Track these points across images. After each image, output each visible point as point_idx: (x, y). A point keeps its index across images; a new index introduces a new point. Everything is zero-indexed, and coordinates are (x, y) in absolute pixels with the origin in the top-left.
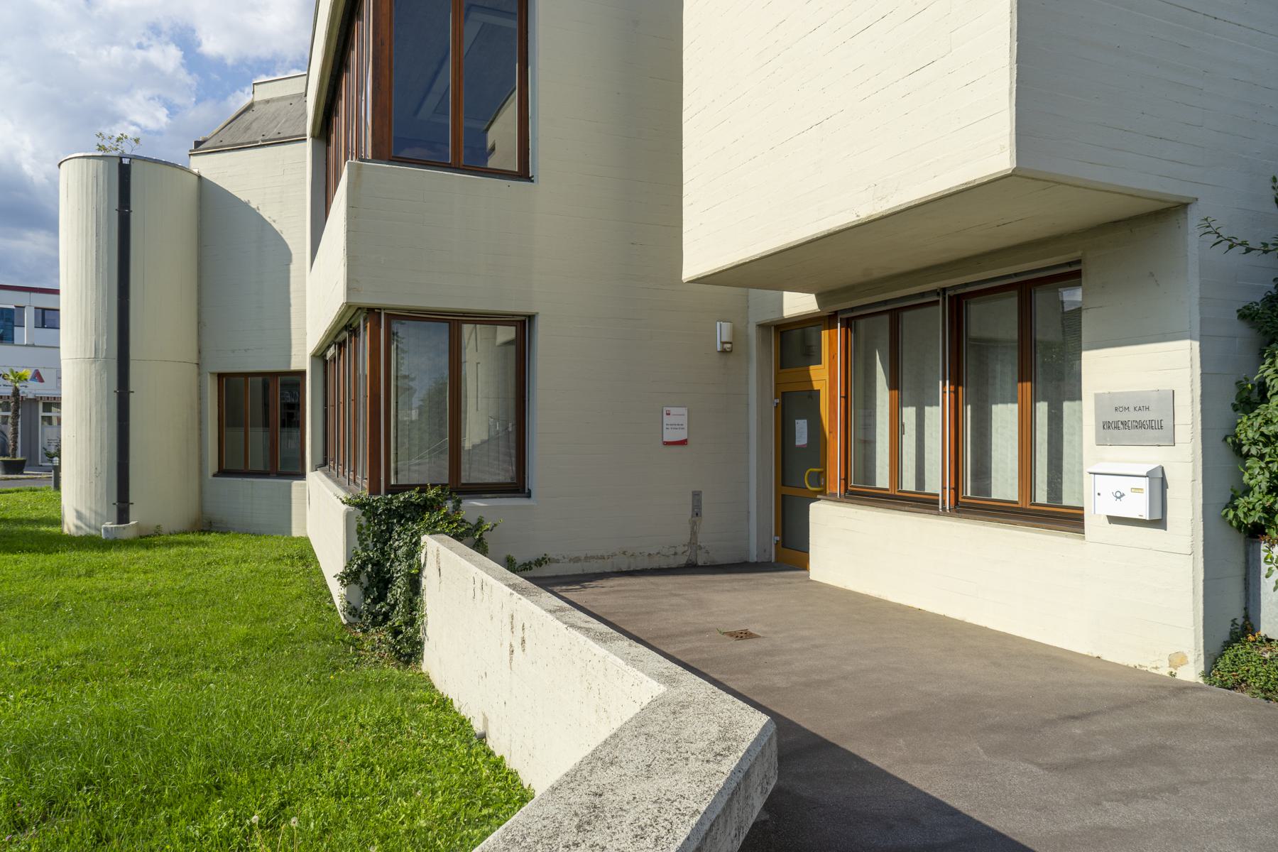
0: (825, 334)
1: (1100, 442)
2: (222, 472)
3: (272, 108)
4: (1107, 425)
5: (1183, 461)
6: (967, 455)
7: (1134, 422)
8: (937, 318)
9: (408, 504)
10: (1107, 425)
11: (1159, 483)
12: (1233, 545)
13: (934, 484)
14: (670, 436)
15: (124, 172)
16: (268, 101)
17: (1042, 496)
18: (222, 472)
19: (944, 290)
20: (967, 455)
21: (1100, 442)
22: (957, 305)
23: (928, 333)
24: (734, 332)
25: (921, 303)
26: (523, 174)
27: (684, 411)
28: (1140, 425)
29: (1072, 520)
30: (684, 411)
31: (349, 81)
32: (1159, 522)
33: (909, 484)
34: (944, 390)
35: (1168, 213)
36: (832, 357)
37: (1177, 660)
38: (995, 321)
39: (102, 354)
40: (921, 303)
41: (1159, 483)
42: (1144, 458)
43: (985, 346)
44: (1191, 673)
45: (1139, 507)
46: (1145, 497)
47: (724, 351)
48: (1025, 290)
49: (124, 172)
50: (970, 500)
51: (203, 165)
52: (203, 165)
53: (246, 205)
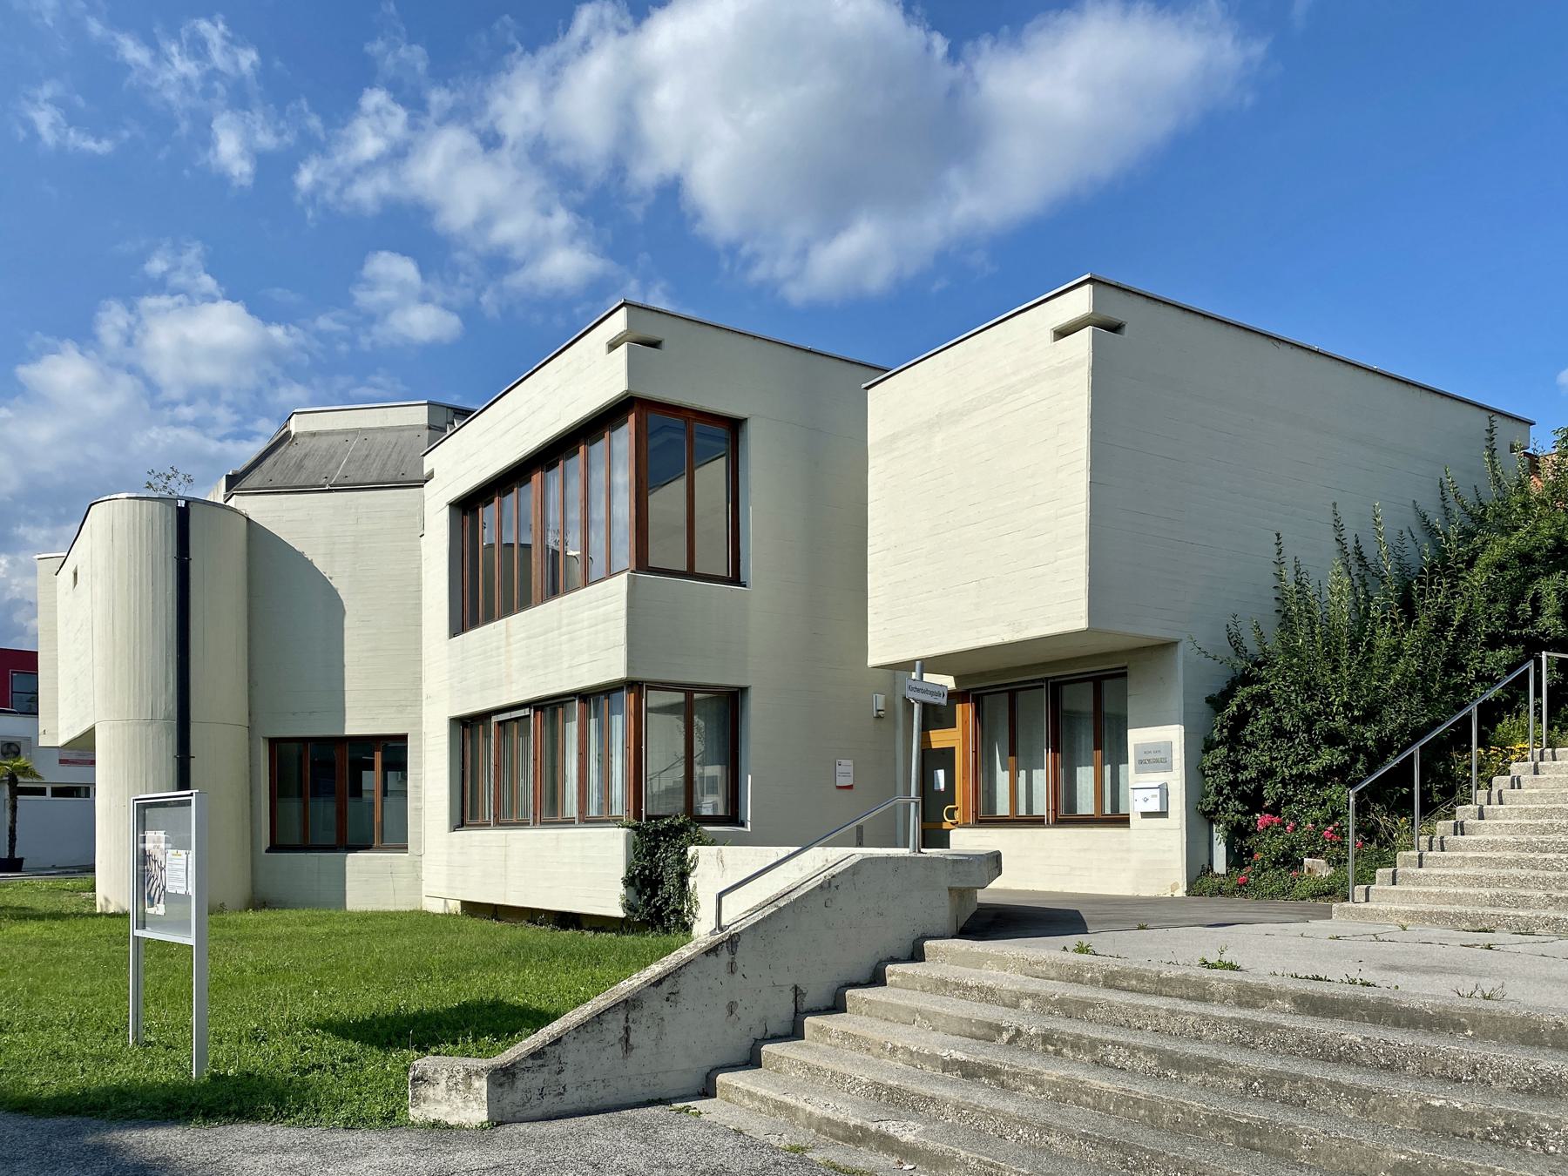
0: (959, 707)
1: (1137, 771)
2: (274, 847)
3: (324, 443)
4: (1141, 762)
5: (1176, 779)
6: (1064, 795)
7: (1155, 760)
8: (1042, 697)
9: (670, 826)
10: (1141, 762)
11: (1164, 790)
12: (1201, 823)
13: (1041, 808)
14: (842, 781)
15: (183, 516)
16: (314, 434)
17: (1108, 811)
18: (274, 847)
19: (1047, 679)
20: (1064, 795)
21: (1137, 771)
22: (1056, 688)
23: (1036, 710)
24: (886, 703)
25: (1032, 686)
26: (735, 579)
27: (850, 762)
28: (1157, 761)
29: (1124, 821)
30: (850, 762)
31: (569, 490)
32: (1163, 814)
33: (1022, 812)
34: (1048, 756)
35: (1168, 646)
36: (965, 722)
37: (1175, 887)
38: (1080, 700)
39: (160, 714)
40: (1032, 686)
41: (1164, 790)
42: (1156, 778)
43: (1075, 716)
44: (1181, 892)
45: (1155, 806)
46: (1157, 801)
47: (879, 717)
48: (1098, 681)
49: (183, 516)
50: (1065, 816)
51: (251, 506)
52: (251, 506)
53: (301, 555)
